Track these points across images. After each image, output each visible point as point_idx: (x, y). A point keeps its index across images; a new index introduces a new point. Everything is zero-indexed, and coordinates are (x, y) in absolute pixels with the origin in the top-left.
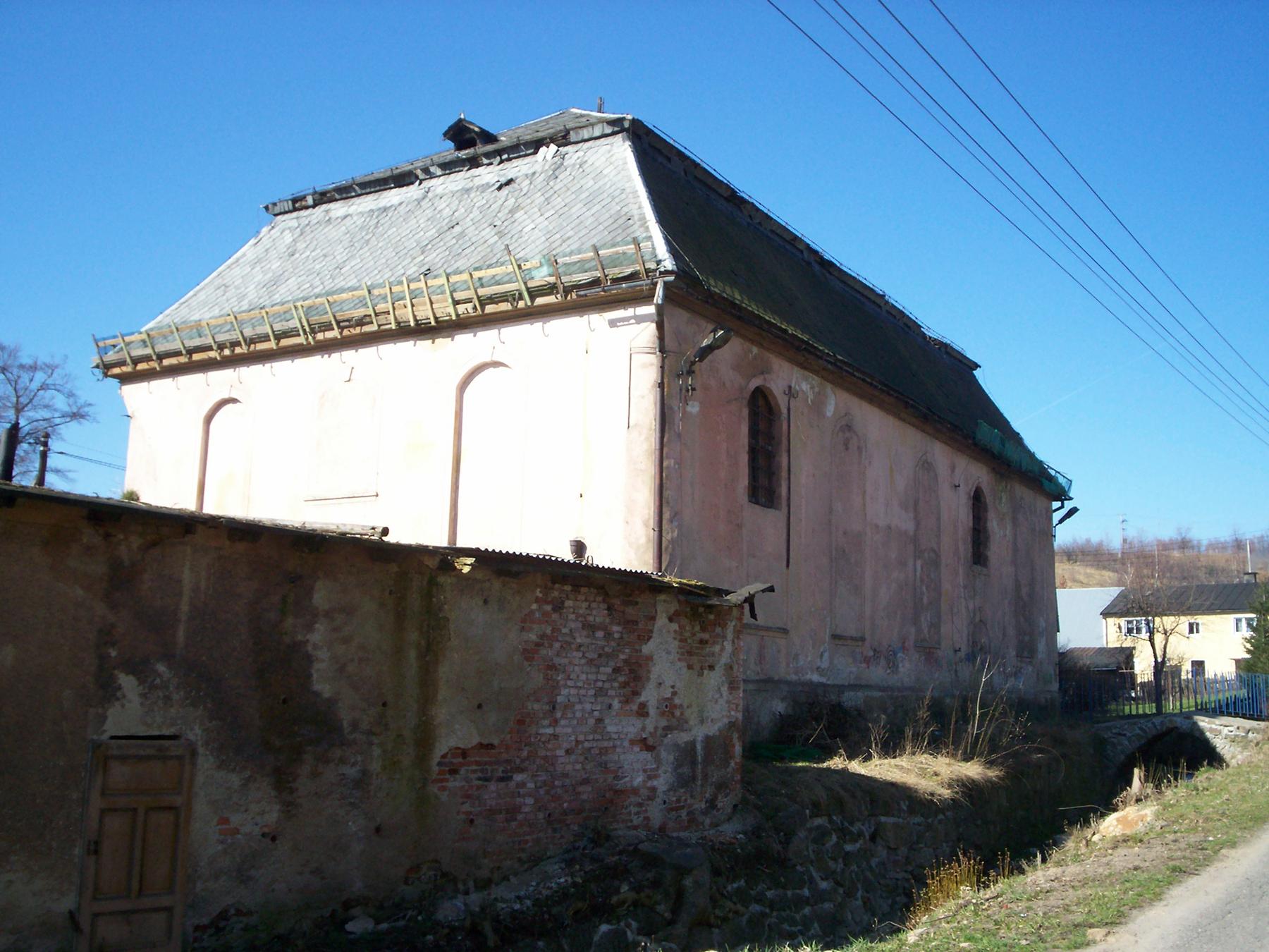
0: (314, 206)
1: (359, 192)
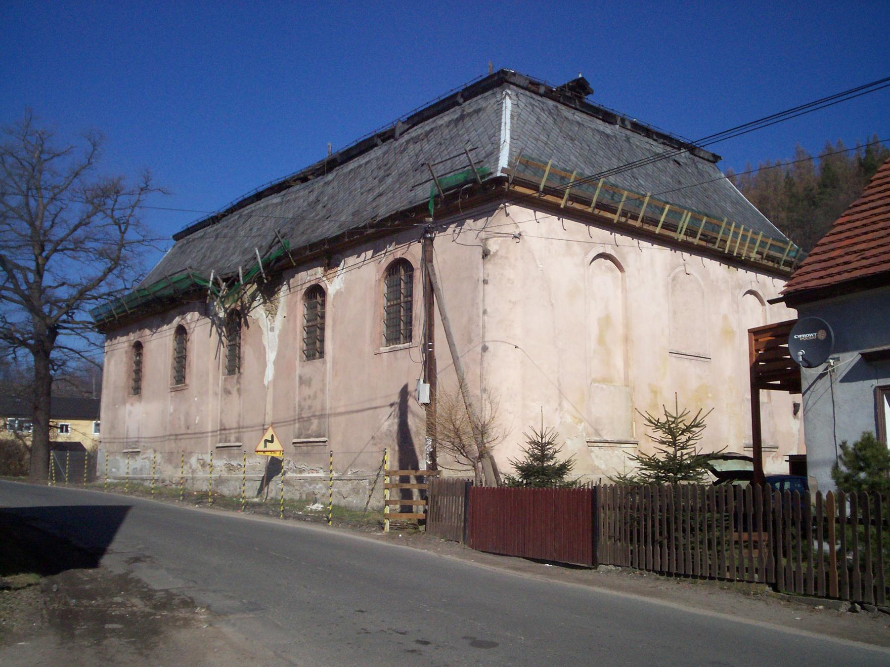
0: (541, 95)
1: (578, 107)
